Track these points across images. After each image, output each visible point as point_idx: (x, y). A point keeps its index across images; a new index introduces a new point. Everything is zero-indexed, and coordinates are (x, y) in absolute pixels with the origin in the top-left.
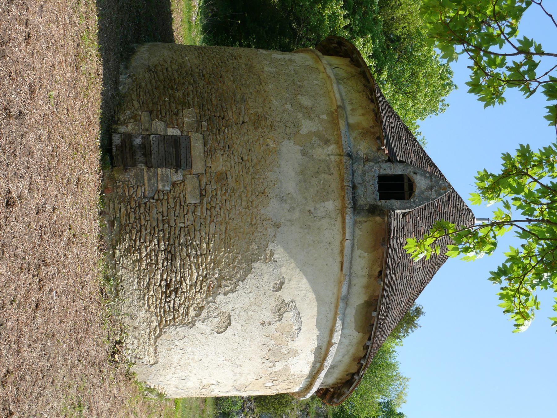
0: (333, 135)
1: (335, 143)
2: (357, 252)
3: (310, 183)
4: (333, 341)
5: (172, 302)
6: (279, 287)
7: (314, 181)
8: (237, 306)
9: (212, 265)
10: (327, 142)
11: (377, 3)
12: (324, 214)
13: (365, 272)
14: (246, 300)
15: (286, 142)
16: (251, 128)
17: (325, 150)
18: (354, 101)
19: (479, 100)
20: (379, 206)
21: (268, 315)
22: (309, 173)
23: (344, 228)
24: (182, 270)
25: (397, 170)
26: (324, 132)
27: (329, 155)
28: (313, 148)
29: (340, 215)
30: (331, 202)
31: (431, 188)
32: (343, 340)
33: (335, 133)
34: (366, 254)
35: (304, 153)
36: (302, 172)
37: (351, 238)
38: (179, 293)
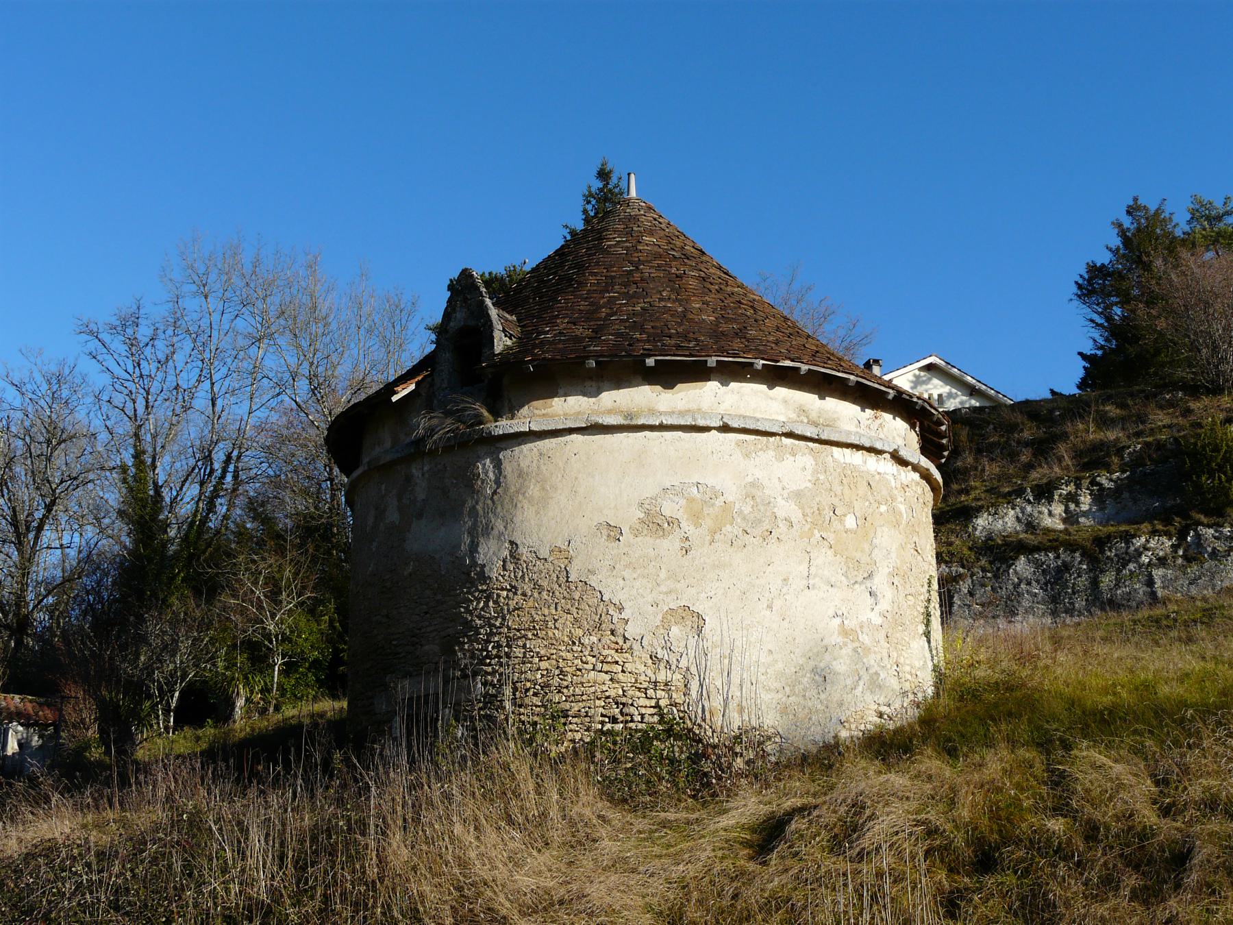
5: (643, 711)
6: (614, 532)
8: (650, 599)
9: (575, 648)
10: (409, 479)
11: (1062, 449)
14: (637, 584)
19: (1076, 283)
21: (669, 545)
24: (584, 697)
29: (498, 445)
35: (420, 516)
38: (624, 700)
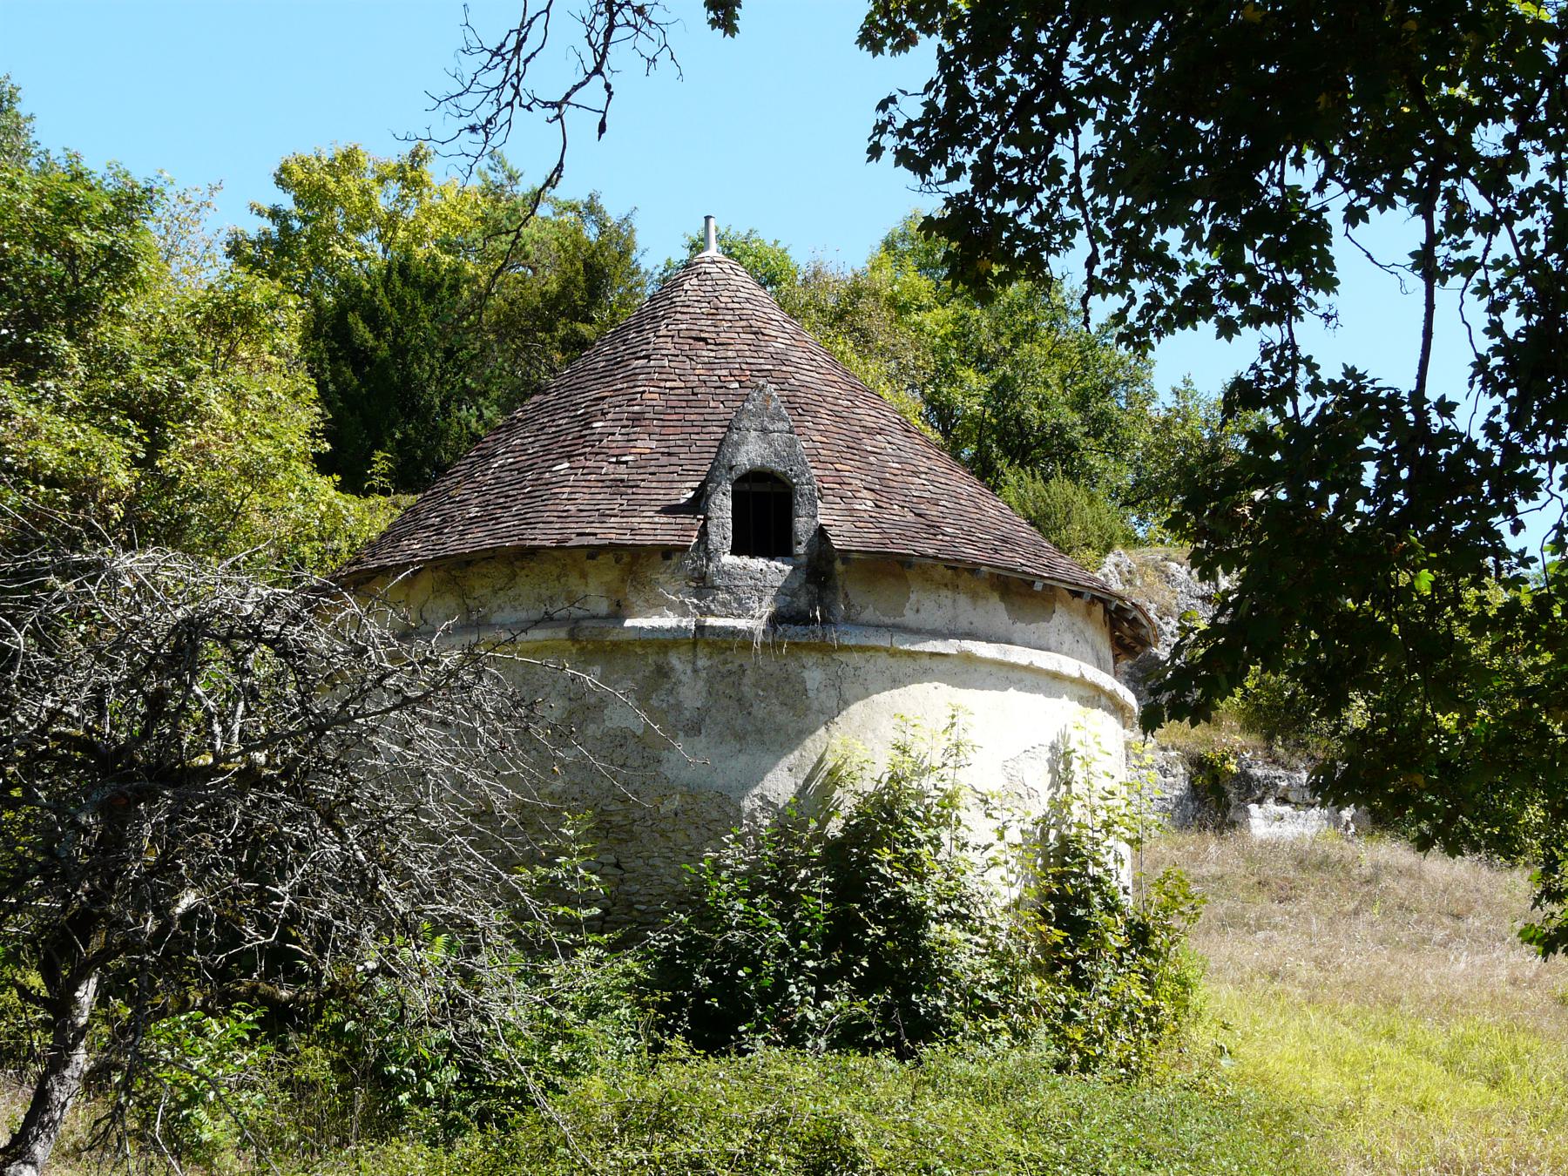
0: (645, 655)
1: (666, 653)
2: (909, 618)
3: (763, 720)
4: (1076, 675)
7: (759, 711)
12: (833, 693)
13: (946, 596)
15: (667, 770)
16: (632, 847)
17: (684, 678)
18: (543, 591)
20: (810, 560)
22: (740, 721)
23: (862, 649)
25: (722, 506)
26: (639, 676)
27: (695, 671)
28: (678, 707)
29: (835, 656)
30: (806, 674)
31: (764, 431)
32: (1065, 647)
33: (639, 650)
34: (913, 597)
36: (740, 737)
37: (888, 635)
